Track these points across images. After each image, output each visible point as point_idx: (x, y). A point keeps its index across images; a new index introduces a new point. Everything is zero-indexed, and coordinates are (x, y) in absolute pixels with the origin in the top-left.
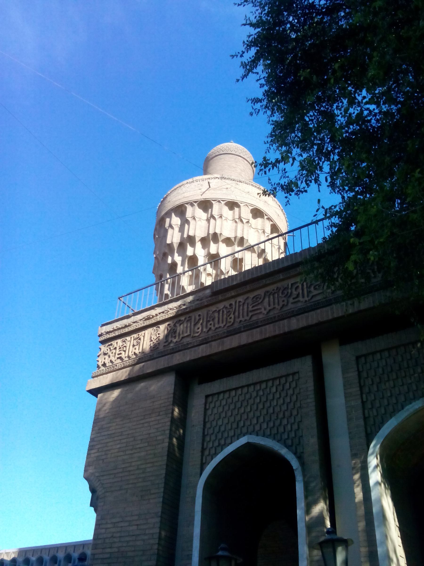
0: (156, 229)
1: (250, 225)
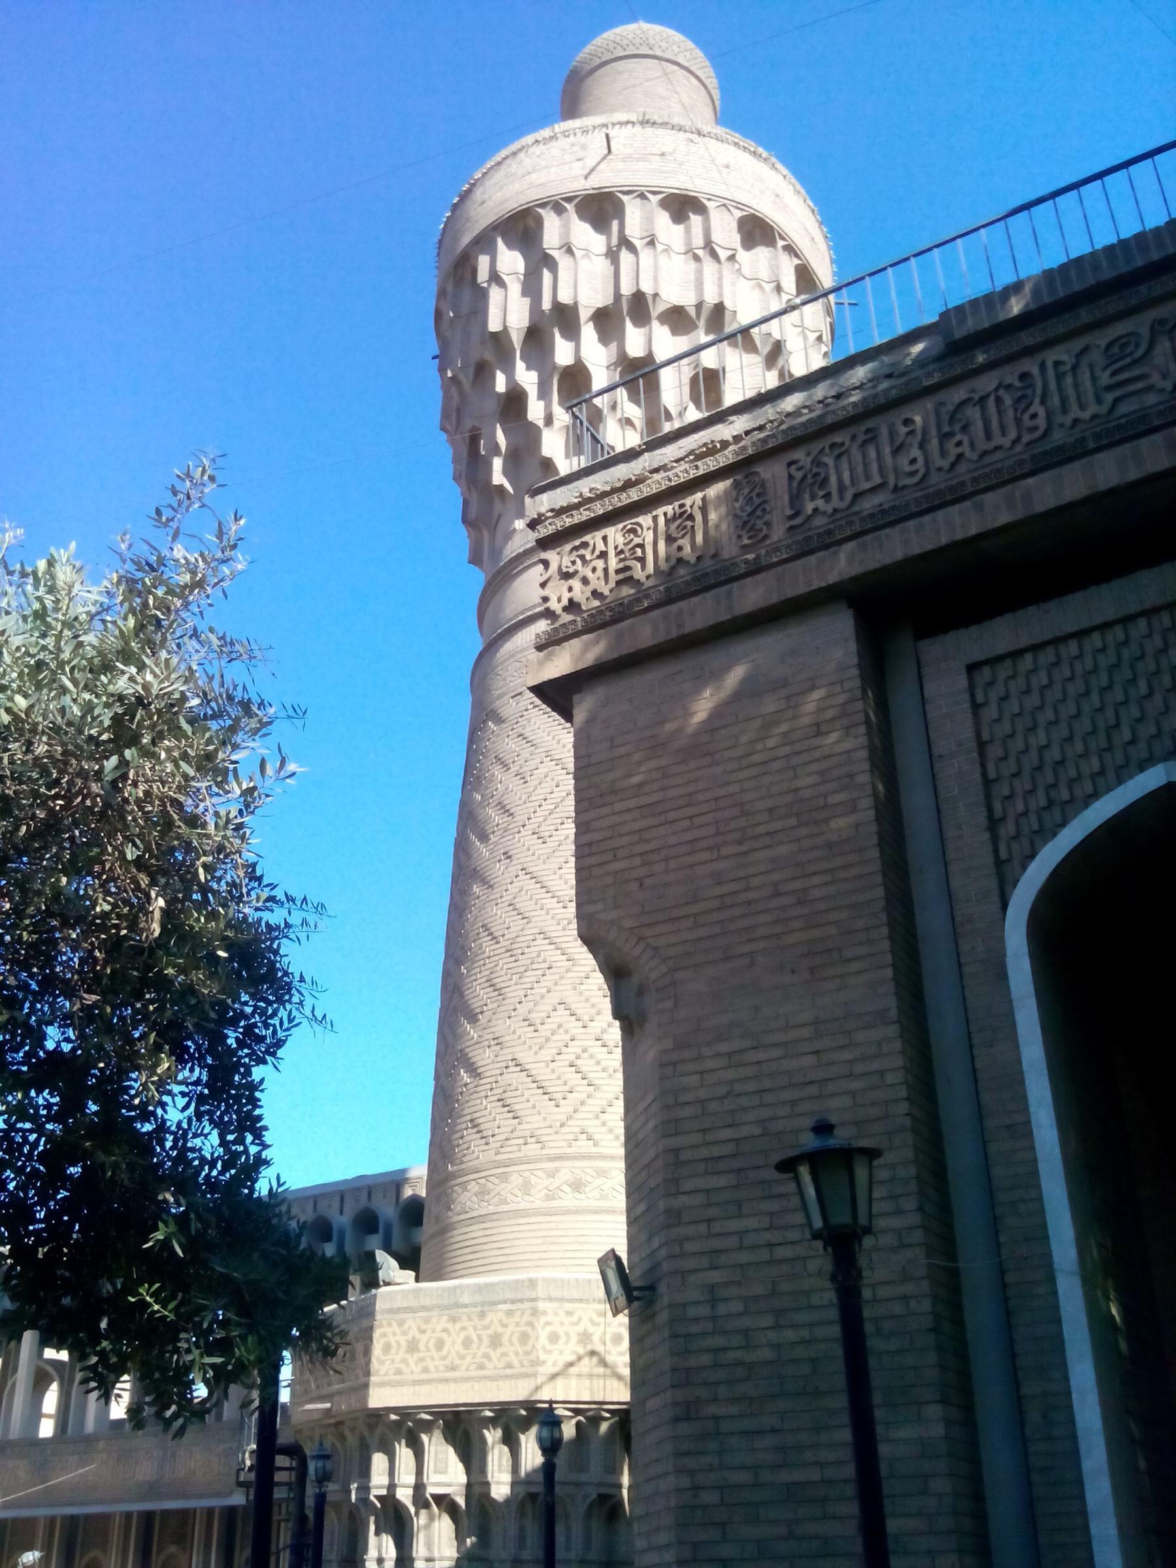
0: (442, 294)
1: (737, 266)
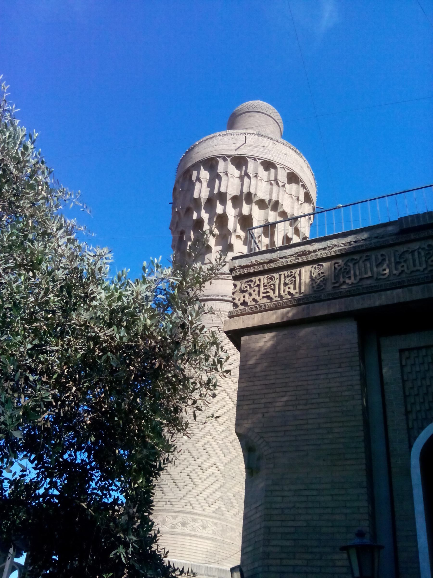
0: (177, 182)
1: (285, 189)
